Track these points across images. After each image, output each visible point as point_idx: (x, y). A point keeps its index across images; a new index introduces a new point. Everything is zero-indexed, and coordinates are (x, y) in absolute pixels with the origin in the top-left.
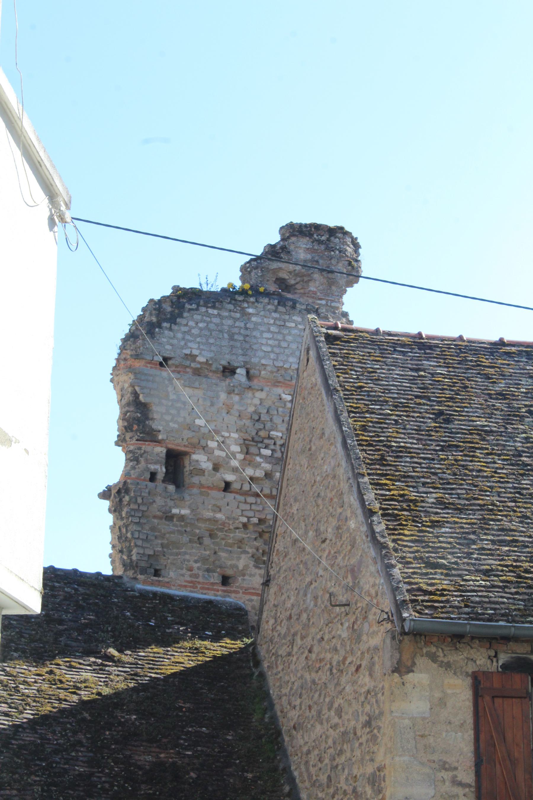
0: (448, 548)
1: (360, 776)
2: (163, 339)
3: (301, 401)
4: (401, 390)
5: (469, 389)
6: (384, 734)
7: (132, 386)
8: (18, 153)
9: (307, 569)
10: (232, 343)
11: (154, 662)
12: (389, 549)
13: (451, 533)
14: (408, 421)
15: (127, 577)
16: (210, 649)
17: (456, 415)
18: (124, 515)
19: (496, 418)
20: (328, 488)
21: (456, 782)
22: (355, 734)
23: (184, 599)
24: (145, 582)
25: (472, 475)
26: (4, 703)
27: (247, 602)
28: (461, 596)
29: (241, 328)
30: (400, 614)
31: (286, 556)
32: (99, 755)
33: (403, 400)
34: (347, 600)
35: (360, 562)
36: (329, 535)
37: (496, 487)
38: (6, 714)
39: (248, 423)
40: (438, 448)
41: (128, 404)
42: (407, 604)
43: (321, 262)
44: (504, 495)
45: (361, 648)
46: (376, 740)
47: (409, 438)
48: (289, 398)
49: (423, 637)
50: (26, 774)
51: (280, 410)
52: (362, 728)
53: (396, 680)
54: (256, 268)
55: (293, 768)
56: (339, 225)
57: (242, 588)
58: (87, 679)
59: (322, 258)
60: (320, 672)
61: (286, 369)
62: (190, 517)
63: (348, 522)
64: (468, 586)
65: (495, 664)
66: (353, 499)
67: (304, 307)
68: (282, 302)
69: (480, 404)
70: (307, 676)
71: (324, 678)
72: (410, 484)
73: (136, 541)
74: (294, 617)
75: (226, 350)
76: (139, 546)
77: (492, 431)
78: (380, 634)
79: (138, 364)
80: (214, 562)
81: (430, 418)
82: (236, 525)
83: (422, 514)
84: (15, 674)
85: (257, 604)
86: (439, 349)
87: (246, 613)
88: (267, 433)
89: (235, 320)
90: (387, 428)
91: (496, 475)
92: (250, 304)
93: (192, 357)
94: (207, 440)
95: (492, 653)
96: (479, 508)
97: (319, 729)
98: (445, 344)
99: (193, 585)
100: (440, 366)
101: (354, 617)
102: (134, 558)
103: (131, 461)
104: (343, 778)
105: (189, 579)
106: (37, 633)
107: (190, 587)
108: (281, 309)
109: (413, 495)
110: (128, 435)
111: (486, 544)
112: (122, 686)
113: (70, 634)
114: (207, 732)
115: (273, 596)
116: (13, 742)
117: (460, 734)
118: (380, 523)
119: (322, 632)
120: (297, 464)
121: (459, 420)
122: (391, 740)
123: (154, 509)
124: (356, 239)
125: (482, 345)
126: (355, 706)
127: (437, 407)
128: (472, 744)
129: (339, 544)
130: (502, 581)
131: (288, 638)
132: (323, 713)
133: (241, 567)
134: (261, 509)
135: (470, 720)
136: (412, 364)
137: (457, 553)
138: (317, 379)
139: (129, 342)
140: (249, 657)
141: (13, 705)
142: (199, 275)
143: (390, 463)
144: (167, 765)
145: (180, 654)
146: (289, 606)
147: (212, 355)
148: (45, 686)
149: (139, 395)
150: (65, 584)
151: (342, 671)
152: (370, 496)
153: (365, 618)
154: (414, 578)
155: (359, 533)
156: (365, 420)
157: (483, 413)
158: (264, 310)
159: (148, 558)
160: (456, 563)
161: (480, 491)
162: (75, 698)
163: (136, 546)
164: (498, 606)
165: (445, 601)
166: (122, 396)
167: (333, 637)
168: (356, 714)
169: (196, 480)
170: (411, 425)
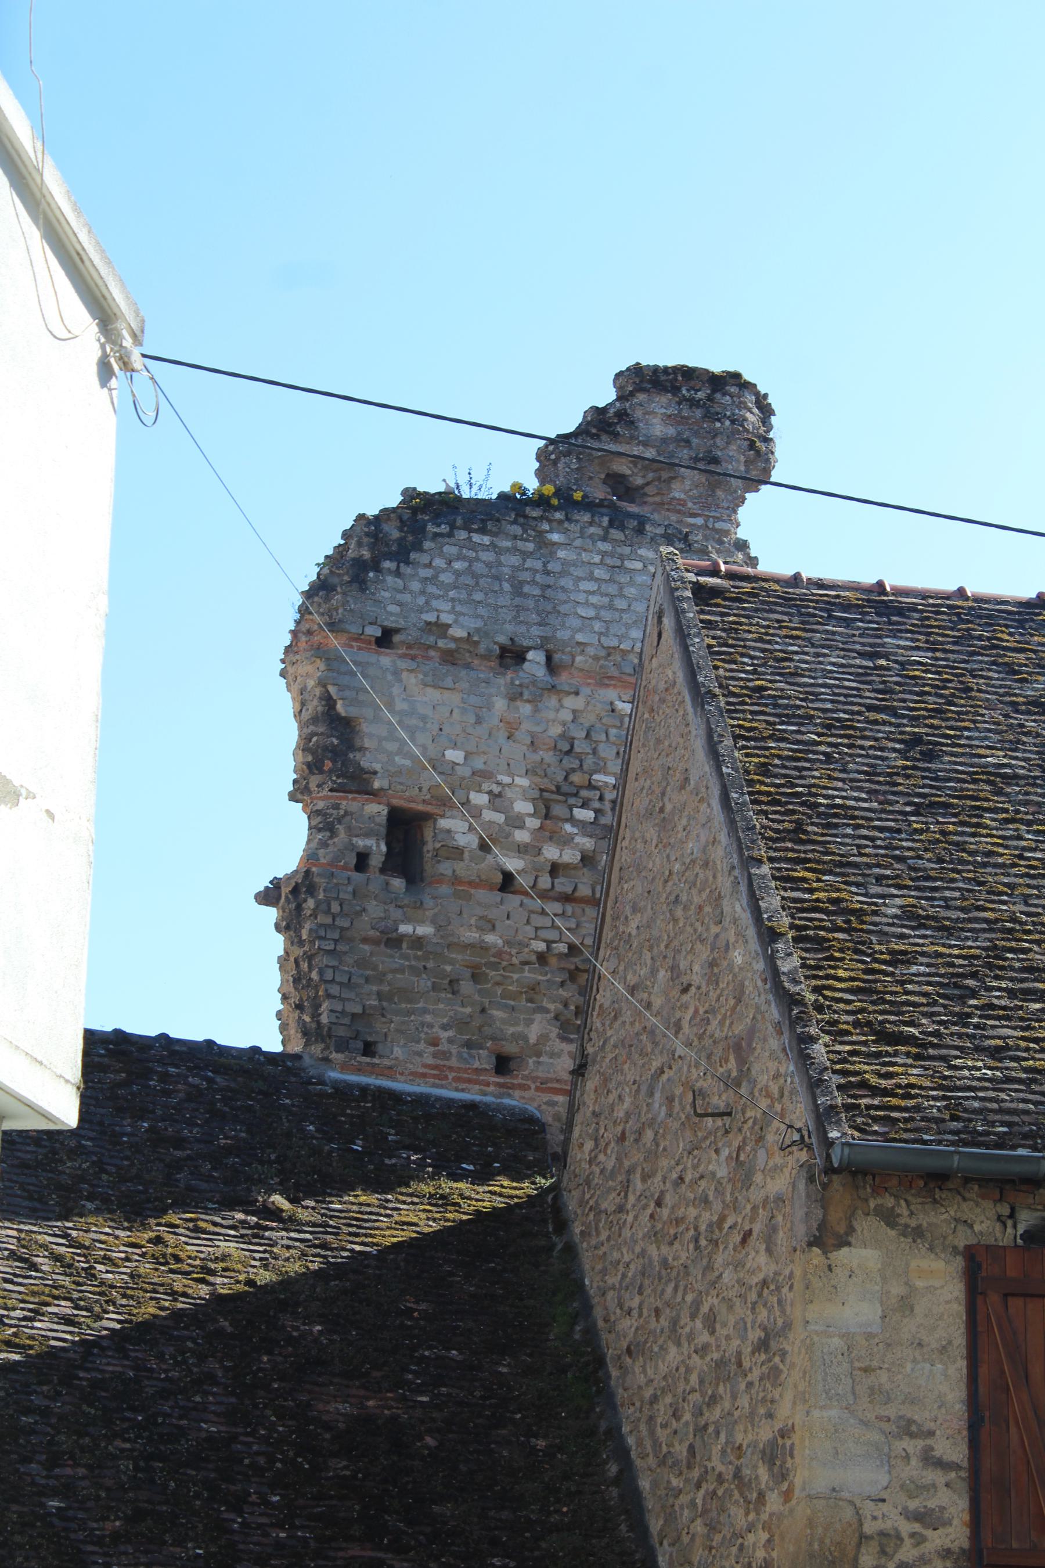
0: (923, 1005)
1: (748, 1446)
2: (383, 593)
3: (646, 716)
4: (839, 695)
5: (973, 694)
6: (793, 1365)
7: (322, 683)
8: (34, 234)
9: (655, 1044)
10: (518, 601)
11: (359, 1222)
12: (805, 1005)
13: (929, 975)
14: (850, 755)
15: (311, 1056)
16: (470, 1199)
17: (947, 745)
18: (304, 937)
19: (1025, 751)
20: (695, 884)
21: (930, 1460)
22: (740, 1364)
23: (421, 1101)
24: (344, 1068)
25: (975, 861)
26: (65, 1299)
27: (544, 1107)
28: (944, 1098)
29: (537, 571)
30: (823, 1133)
31: (616, 1018)
32: (247, 1402)
33: (842, 715)
34: (728, 1105)
35: (752, 1031)
36: (694, 977)
37: (1020, 885)
38: (68, 1321)
39: (549, 757)
40: (908, 809)
41: (315, 720)
42: (838, 1113)
43: (695, 441)
44: (1036, 902)
45: (752, 1198)
46: (777, 1377)
47: (852, 789)
48: (627, 708)
49: (869, 1178)
50: (105, 1435)
51: (613, 732)
52: (753, 1353)
53: (815, 1261)
54: (567, 454)
55: (625, 1429)
56: (731, 369)
57: (534, 1079)
58: (226, 1254)
59: (696, 434)
60: (677, 1245)
61: (624, 653)
62: (435, 941)
63: (730, 953)
64: (959, 1079)
65: (1010, 1230)
66: (738, 908)
67: (660, 531)
68: (618, 520)
69: (994, 723)
70: (653, 1251)
71: (684, 1255)
72: (852, 879)
73: (329, 986)
74: (631, 1138)
75: (507, 615)
76: (334, 997)
77: (1016, 776)
78: (787, 1171)
79: (334, 642)
80: (480, 1029)
81: (895, 750)
82: (525, 956)
83: (874, 939)
84: (87, 1244)
85: (563, 1111)
86: (916, 615)
87: (543, 1127)
88: (587, 777)
89: (525, 555)
90: (809, 769)
91: (1022, 863)
92: (555, 524)
93: (440, 628)
94: (469, 790)
95: (1005, 1210)
96: (985, 926)
97: (673, 1354)
98: (929, 605)
99: (440, 1073)
100: (918, 648)
101: (740, 1138)
102: (324, 1019)
103: (320, 830)
104: (716, 1450)
105: (430, 1061)
106: (133, 1164)
107: (434, 1076)
108: (615, 534)
109: (857, 901)
110: (314, 781)
111: (997, 997)
112: (295, 1268)
113: (196, 1167)
114: (460, 1358)
115: (592, 1096)
116: (82, 1374)
117: (939, 1366)
118: (790, 954)
119: (681, 1167)
120: (638, 838)
121: (952, 754)
122: (804, 1377)
123: (364, 926)
124: (766, 396)
125: (1003, 607)
126: (741, 1310)
127: (909, 729)
128: (963, 1386)
129: (713, 995)
130: (1026, 1070)
131: (620, 1179)
132: (682, 1323)
133: (533, 1039)
134: (574, 926)
135: (959, 1339)
136: (863, 644)
137: (939, 1014)
138: (676, 672)
139: (316, 599)
140: (547, 1214)
141: (82, 1303)
142: (454, 467)
143: (814, 837)
144: (380, 1422)
145: (412, 1207)
146: (621, 1114)
147: (479, 624)
148: (145, 1267)
149: (335, 702)
150: (189, 1069)
151: (716, 1243)
152: (772, 901)
153: (760, 1139)
154: (854, 1063)
155: (749, 975)
156: (767, 753)
157: (999, 741)
158: (581, 537)
159: (352, 1020)
160: (936, 1034)
161: (988, 893)
162: (204, 1290)
163: (329, 996)
164: (1016, 1119)
165: (913, 1107)
166: (303, 704)
167: (702, 1177)
168: (742, 1327)
169: (446, 868)
170: (857, 763)
